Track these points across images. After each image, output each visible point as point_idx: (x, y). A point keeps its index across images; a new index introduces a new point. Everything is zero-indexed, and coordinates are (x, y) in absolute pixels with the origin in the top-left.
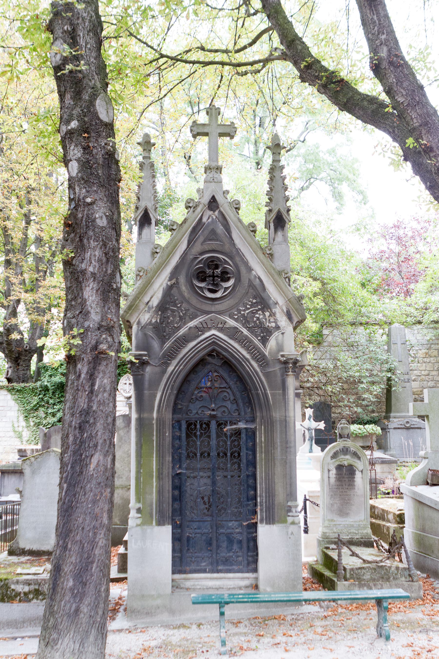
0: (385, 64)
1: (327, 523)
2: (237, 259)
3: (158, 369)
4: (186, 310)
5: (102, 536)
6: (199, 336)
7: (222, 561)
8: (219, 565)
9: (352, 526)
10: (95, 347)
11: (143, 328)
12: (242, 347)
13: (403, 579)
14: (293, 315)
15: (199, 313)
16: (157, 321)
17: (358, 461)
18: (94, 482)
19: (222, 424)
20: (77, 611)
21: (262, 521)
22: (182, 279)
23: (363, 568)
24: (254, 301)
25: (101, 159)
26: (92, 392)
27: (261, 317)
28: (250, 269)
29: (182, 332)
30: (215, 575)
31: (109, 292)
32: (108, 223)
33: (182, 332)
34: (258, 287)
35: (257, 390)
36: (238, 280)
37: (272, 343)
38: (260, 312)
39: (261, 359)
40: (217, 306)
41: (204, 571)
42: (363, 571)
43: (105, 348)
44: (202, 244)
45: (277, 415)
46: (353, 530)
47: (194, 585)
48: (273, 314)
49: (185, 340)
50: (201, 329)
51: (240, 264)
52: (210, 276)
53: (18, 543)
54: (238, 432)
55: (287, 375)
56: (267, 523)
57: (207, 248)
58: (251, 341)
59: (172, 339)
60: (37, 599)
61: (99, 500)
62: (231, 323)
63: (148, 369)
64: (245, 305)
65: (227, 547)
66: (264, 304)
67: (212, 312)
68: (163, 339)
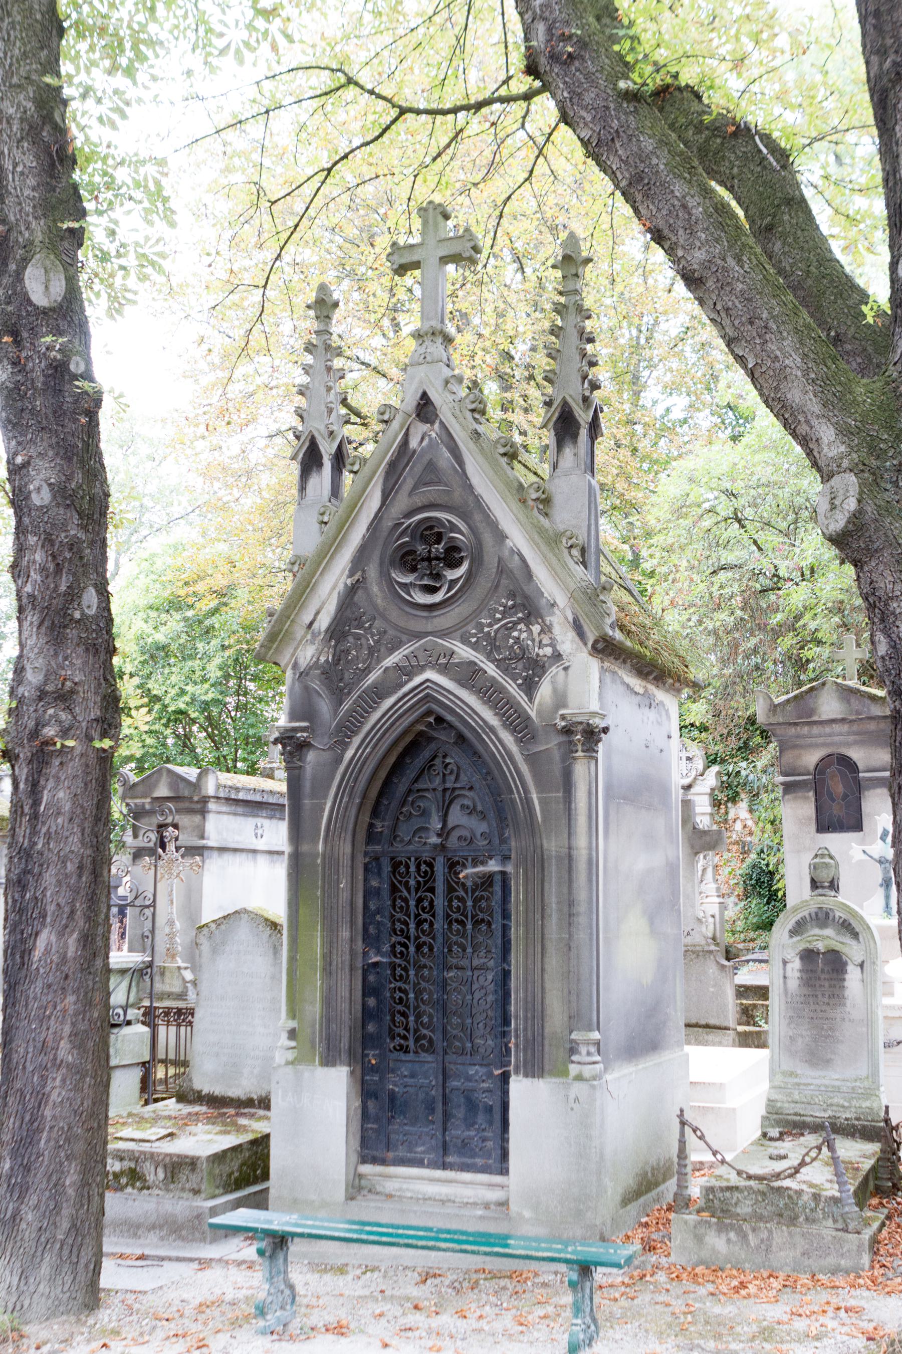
0: (543, 61)
1: (779, 1079)
2: (477, 517)
3: (327, 756)
4: (379, 633)
5: (58, 1082)
6: (402, 685)
7: (455, 1146)
8: (448, 1154)
9: (838, 1089)
10: (35, 734)
11: (302, 675)
12: (485, 703)
13: (830, 1223)
14: (586, 628)
15: (404, 638)
16: (327, 661)
17: (854, 942)
18: (39, 984)
19: (458, 863)
20: (16, 1216)
21: (517, 1072)
22: (373, 571)
23: (737, 1188)
24: (510, 603)
25: (41, 379)
26: (35, 816)
27: (524, 635)
28: (501, 537)
29: (372, 677)
30: (439, 1173)
31: (65, 627)
32: (54, 497)
33: (372, 677)
34: (516, 572)
35: (512, 792)
36: (477, 561)
37: (544, 691)
38: (522, 626)
39: (520, 725)
40: (436, 621)
41: (419, 1163)
42: (736, 1194)
43: (52, 733)
44: (410, 494)
45: (552, 845)
46: (838, 1100)
47: (400, 1190)
48: (547, 629)
49: (378, 693)
50: (406, 671)
51: (481, 527)
52: (423, 560)
53: (191, 1080)
54: (487, 880)
55: (575, 759)
56: (526, 1075)
57: (418, 501)
58: (502, 690)
59: (355, 696)
60: (133, 1187)
61: (49, 1017)
62: (464, 652)
63: (311, 756)
64: (492, 613)
65: (465, 1119)
66: (529, 608)
67: (427, 634)
68: (338, 695)
